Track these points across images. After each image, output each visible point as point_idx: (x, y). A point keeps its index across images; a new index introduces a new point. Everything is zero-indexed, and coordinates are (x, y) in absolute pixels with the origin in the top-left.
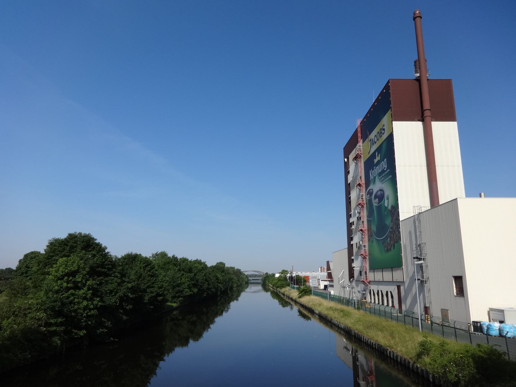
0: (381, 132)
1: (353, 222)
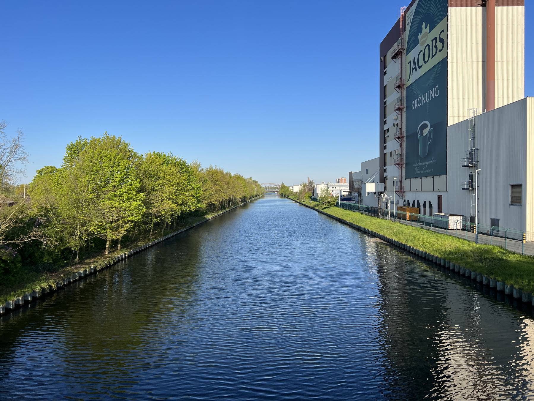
0: (436, 47)
1: (388, 129)
